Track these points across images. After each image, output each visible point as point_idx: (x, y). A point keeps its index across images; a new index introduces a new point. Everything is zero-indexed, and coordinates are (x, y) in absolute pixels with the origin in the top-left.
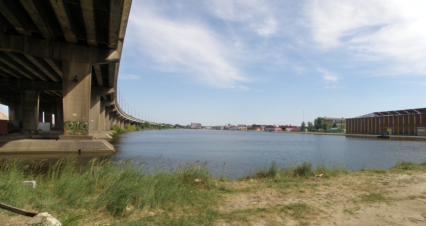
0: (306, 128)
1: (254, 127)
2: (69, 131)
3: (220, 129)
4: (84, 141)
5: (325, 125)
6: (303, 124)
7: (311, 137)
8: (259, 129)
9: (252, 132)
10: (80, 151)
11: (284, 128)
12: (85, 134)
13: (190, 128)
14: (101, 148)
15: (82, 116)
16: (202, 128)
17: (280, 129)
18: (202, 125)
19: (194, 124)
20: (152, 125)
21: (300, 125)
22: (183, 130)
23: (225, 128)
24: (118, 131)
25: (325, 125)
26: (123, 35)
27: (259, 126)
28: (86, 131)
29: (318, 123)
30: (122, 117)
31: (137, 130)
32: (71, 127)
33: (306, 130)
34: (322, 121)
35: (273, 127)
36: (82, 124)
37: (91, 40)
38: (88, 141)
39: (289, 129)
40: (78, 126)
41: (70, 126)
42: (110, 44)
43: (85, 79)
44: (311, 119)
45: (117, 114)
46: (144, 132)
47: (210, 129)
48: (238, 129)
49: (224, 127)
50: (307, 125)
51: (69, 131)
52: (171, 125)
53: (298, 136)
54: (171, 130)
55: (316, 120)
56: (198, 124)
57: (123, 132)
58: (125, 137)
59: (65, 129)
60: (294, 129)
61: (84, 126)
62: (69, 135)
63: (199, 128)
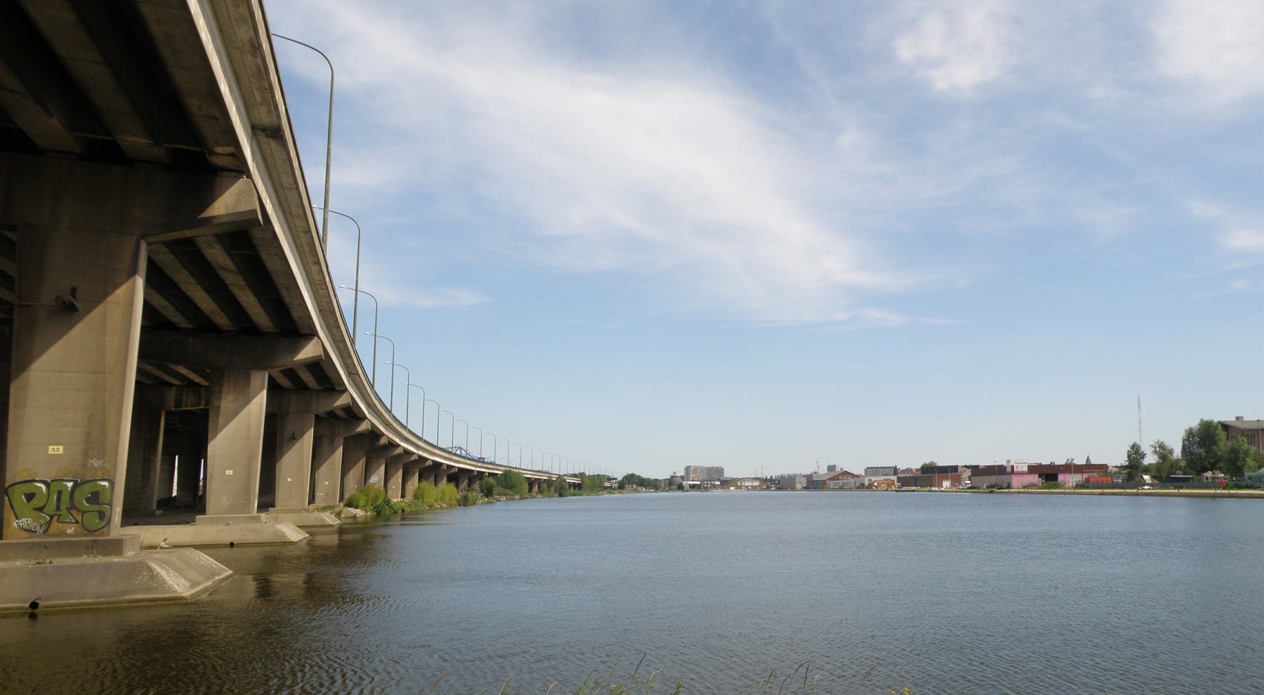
0: (1147, 470)
1: (930, 474)
2: (25, 521)
3: (793, 488)
4: (85, 559)
5: (1235, 451)
6: (1135, 453)
7: (1172, 513)
8: (946, 484)
9: (919, 495)
10: (34, 605)
11: (1049, 475)
12: (92, 532)
13: (681, 487)
14: (133, 591)
15: (86, 455)
16: (726, 483)
17: (1035, 479)
18: (728, 474)
19: (696, 469)
20: (531, 483)
21: (1122, 460)
22: (652, 494)
23: (813, 483)
24: (379, 513)
25: (1235, 451)
26: (269, 112)
27: (950, 471)
28: (102, 515)
29: (1201, 445)
30: (407, 452)
31: (464, 502)
32: (36, 502)
33: (1146, 477)
34: (1222, 435)
35: (1000, 470)
36: (87, 490)
37: (132, 139)
38: (101, 559)
39: (1073, 479)
40: (66, 498)
41: (30, 497)
42: (213, 153)
43: (110, 299)
44: (1169, 432)
45: (383, 441)
46: (498, 506)
47: (754, 488)
48: (862, 487)
49: (809, 478)
50: (1150, 459)
51: (25, 521)
52: (609, 479)
53: (1113, 513)
54: (607, 496)
55: (1190, 433)
56: (709, 469)
57: (406, 516)
58: (384, 537)
59: (8, 513)
60: (1095, 477)
61: (95, 498)
62: (25, 538)
63: (714, 486)
